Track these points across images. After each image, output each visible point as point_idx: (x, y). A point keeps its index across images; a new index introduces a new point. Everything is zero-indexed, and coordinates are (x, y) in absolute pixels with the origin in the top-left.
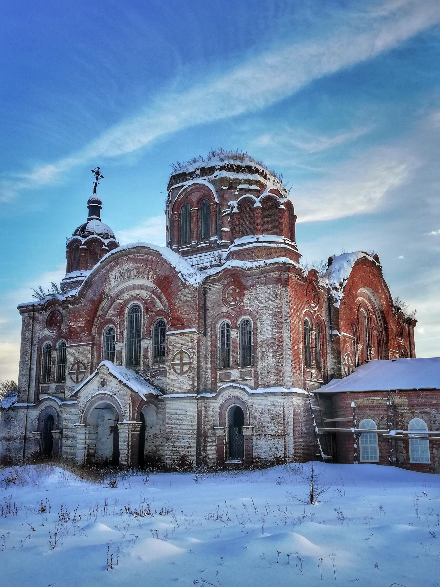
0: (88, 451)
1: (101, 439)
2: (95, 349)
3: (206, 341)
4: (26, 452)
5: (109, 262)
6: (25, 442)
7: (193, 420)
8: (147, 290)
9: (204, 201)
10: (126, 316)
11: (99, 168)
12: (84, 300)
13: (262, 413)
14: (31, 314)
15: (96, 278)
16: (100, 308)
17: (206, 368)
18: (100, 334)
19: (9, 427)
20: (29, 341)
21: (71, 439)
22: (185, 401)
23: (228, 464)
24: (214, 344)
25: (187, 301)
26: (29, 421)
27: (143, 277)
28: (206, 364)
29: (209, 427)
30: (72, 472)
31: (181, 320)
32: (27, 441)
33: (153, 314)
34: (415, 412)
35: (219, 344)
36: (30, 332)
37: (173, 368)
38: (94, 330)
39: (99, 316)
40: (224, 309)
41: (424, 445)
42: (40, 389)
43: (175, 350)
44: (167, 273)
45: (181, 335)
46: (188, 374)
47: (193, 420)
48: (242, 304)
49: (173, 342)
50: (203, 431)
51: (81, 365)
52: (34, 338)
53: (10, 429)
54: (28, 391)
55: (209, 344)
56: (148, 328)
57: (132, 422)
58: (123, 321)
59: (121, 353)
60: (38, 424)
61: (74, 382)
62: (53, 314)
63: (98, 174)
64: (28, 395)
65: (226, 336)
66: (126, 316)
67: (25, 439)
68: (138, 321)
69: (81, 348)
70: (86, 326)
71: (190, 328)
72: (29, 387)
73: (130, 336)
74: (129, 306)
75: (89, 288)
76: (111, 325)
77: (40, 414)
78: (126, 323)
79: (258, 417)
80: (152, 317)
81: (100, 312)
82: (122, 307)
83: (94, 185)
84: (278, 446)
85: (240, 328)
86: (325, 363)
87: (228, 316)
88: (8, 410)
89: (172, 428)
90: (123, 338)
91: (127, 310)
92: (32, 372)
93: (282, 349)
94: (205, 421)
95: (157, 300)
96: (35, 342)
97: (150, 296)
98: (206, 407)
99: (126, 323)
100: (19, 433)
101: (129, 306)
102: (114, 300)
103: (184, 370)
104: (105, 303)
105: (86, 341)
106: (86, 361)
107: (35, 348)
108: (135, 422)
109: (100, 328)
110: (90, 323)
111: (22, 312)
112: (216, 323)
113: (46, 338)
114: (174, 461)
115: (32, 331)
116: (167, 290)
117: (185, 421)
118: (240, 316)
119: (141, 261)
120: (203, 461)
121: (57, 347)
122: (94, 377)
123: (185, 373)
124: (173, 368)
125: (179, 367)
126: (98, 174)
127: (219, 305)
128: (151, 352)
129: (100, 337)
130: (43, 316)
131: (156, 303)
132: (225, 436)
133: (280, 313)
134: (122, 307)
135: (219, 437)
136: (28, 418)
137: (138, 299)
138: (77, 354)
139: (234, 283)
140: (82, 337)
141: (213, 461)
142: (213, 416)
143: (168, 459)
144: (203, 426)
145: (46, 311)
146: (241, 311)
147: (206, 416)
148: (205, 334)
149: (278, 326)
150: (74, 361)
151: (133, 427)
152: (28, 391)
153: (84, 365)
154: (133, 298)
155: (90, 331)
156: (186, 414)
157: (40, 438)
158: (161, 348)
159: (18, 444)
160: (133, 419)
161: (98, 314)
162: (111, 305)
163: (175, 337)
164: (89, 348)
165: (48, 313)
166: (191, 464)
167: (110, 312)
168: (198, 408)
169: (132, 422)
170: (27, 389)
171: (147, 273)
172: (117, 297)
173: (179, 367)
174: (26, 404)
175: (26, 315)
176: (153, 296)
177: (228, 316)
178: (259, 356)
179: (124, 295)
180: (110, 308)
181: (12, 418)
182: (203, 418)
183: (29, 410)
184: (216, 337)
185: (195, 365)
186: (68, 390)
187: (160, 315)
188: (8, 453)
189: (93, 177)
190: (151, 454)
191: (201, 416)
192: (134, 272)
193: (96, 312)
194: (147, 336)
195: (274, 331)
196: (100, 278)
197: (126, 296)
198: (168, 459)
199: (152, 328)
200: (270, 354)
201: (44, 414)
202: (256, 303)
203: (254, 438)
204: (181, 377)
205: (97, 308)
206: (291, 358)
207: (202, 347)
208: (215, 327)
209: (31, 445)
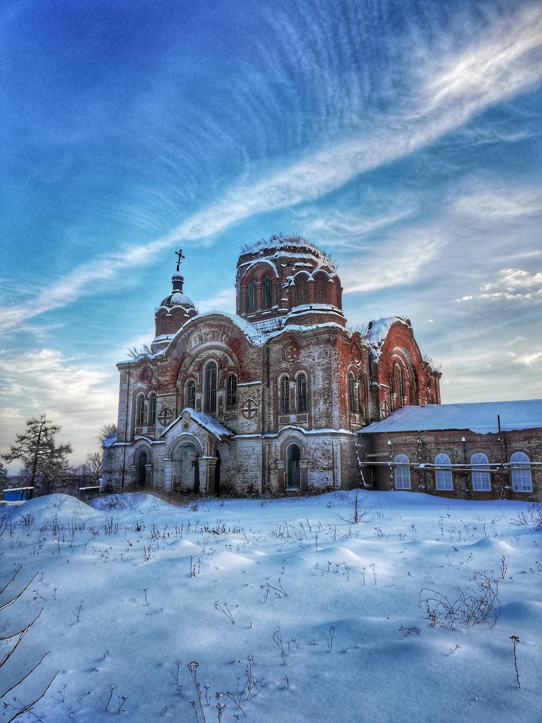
0: (174, 481)
1: (184, 471)
3: (269, 391)
4: (124, 482)
5: (190, 327)
6: (123, 474)
7: (259, 456)
8: (221, 350)
9: (267, 277)
11: (181, 250)
12: (170, 358)
13: (315, 450)
14: (127, 370)
15: (180, 341)
16: (183, 365)
17: (269, 413)
18: (183, 386)
19: (110, 462)
20: (126, 392)
21: (160, 472)
22: (252, 440)
23: (288, 491)
24: (276, 394)
25: (253, 359)
26: (127, 457)
27: (218, 340)
29: (272, 462)
30: (161, 498)
31: (249, 374)
32: (125, 473)
34: (440, 449)
35: (279, 393)
36: (127, 385)
37: (243, 414)
38: (179, 383)
39: (182, 371)
40: (284, 365)
42: (135, 431)
43: (244, 399)
44: (237, 336)
45: (249, 387)
46: (254, 418)
47: (259, 456)
48: (299, 361)
50: (267, 465)
51: (168, 411)
52: (130, 389)
53: (111, 464)
54: (126, 433)
56: (222, 381)
57: (210, 457)
59: (200, 401)
60: (134, 459)
61: (163, 425)
62: (145, 371)
63: (180, 255)
64: (126, 436)
67: (123, 472)
69: (167, 398)
70: (171, 380)
71: (256, 381)
72: (126, 430)
73: (208, 388)
75: (174, 348)
76: (192, 379)
77: (135, 451)
78: (204, 377)
79: (312, 453)
80: (225, 372)
81: (183, 368)
82: (201, 365)
84: (329, 477)
85: (297, 381)
87: (287, 370)
88: (110, 449)
89: (242, 462)
90: (202, 389)
91: (204, 367)
92: (128, 417)
93: (331, 397)
94: (268, 457)
95: (229, 358)
97: (224, 355)
98: (269, 445)
99: (204, 377)
100: (119, 467)
101: (206, 363)
102: (194, 359)
103: (252, 415)
104: (187, 361)
105: (172, 392)
106: (172, 408)
107: (131, 398)
108: (212, 458)
109: (184, 381)
111: (120, 369)
112: (277, 377)
113: (140, 389)
114: (244, 489)
116: (237, 349)
117: (253, 457)
119: (216, 326)
120: (267, 489)
121: (148, 397)
122: (178, 421)
123: (252, 417)
124: (243, 414)
125: (248, 413)
126: (180, 255)
129: (183, 389)
130: (136, 372)
132: (285, 468)
134: (201, 365)
135: (280, 469)
136: (126, 454)
139: (292, 344)
140: (168, 389)
141: (275, 489)
142: (275, 453)
143: (239, 488)
144: (267, 461)
145: (139, 368)
146: (297, 367)
147: (269, 452)
148: (268, 386)
149: (328, 378)
150: (162, 408)
151: (210, 462)
152: (126, 433)
153: (171, 412)
156: (254, 451)
157: (136, 471)
158: (233, 398)
159: (118, 476)
160: (211, 455)
161: (181, 370)
163: (243, 388)
166: (258, 491)
168: (263, 446)
169: (210, 457)
170: (125, 431)
171: (220, 336)
173: (248, 413)
174: (124, 444)
175: (123, 371)
176: (226, 355)
178: (313, 403)
180: (191, 364)
181: (113, 455)
182: (267, 454)
183: (126, 448)
184: (277, 388)
185: (260, 411)
186: (158, 432)
188: (110, 483)
189: (177, 257)
190: (225, 484)
191: (266, 453)
192: (210, 336)
193: (179, 369)
194: (221, 387)
196: (183, 340)
197: (204, 355)
198: (239, 488)
201: (138, 451)
203: (309, 470)
205: (181, 365)
208: (276, 380)
209: (128, 477)
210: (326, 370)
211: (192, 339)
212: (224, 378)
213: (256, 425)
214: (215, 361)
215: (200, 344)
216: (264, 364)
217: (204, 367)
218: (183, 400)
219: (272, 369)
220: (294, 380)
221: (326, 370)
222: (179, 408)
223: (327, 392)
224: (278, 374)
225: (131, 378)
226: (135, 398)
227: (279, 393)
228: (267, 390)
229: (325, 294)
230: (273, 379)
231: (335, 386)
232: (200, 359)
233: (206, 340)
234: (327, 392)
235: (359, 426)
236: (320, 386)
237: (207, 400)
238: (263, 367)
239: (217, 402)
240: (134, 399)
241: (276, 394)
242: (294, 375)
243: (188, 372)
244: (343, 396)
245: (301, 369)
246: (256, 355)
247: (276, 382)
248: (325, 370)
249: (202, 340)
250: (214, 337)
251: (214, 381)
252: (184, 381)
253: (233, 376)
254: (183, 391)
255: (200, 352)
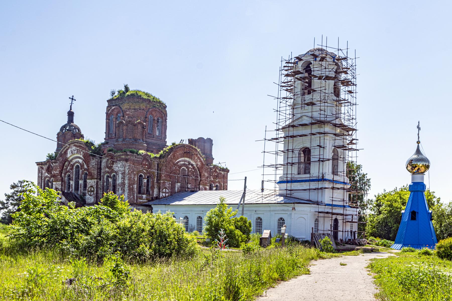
2: (63, 183)
3: (101, 183)
9: (119, 115)
10: (74, 170)
11: (73, 96)
14: (41, 166)
15: (63, 153)
16: (65, 165)
17: (100, 193)
18: (65, 176)
20: (40, 178)
24: (103, 184)
25: (93, 165)
27: (79, 154)
28: (100, 192)
30: (349, 248)
33: (83, 170)
35: (105, 184)
36: (41, 174)
38: (63, 175)
41: (281, 224)
48: (113, 168)
49: (89, 182)
55: (102, 184)
56: (82, 175)
58: (73, 172)
59: (72, 185)
63: (72, 99)
65: (107, 180)
66: (74, 170)
68: (79, 172)
70: (59, 173)
73: (76, 178)
74: (75, 165)
78: (74, 173)
80: (83, 171)
81: (65, 168)
83: (71, 105)
86: (153, 192)
87: (108, 172)
90: (73, 179)
91: (74, 167)
93: (124, 187)
96: (43, 178)
99: (74, 173)
101: (75, 165)
103: (92, 194)
107: (43, 181)
109: (65, 174)
110: (61, 172)
111: (37, 165)
112: (104, 175)
113: (47, 177)
115: (42, 173)
118: (112, 173)
123: (92, 195)
126: (72, 99)
127: (105, 168)
128: (82, 186)
129: (65, 178)
130: (45, 167)
131: (84, 165)
133: (124, 173)
134: (72, 166)
137: (78, 163)
138: (56, 185)
145: (47, 165)
146: (113, 171)
148: (100, 180)
149: (123, 178)
154: (76, 162)
155: (61, 175)
161: (64, 168)
162: (69, 164)
164: (60, 183)
165: (47, 166)
167: (69, 168)
172: (71, 161)
175: (39, 166)
176: (83, 162)
177: (108, 172)
178: (117, 189)
179: (73, 161)
180: (69, 166)
184: (104, 181)
185: (95, 192)
187: (86, 170)
189: (70, 100)
192: (76, 152)
193: (63, 167)
194: (81, 179)
195: (122, 180)
197: (74, 161)
199: (83, 176)
200: (120, 189)
202: (117, 168)
204: (91, 197)
206: (128, 191)
207: (99, 185)
208: (104, 177)
210: (122, 174)
211: (68, 152)
212: (83, 174)
213: (93, 199)
214: (79, 165)
215: (72, 155)
216: (98, 168)
217: (74, 167)
218: (65, 184)
219: (102, 171)
220: (111, 178)
221: (122, 174)
222: (63, 188)
223: (123, 184)
224: (105, 174)
225: (43, 170)
226: (45, 181)
227: (105, 184)
228: (100, 181)
229: (133, 132)
230: (102, 176)
231: (126, 182)
232: (72, 163)
233: (74, 154)
234: (123, 184)
235: (146, 201)
236: (120, 181)
237: (75, 185)
238: (97, 170)
239: (79, 186)
240: (44, 181)
241: (103, 184)
242: (111, 175)
243: (68, 170)
244: (131, 187)
245: (114, 172)
246: (94, 163)
247: (104, 178)
248: (122, 174)
249: (72, 153)
250: (77, 152)
251: (78, 176)
252: (65, 174)
253: (87, 173)
254: (65, 180)
255: (72, 159)
